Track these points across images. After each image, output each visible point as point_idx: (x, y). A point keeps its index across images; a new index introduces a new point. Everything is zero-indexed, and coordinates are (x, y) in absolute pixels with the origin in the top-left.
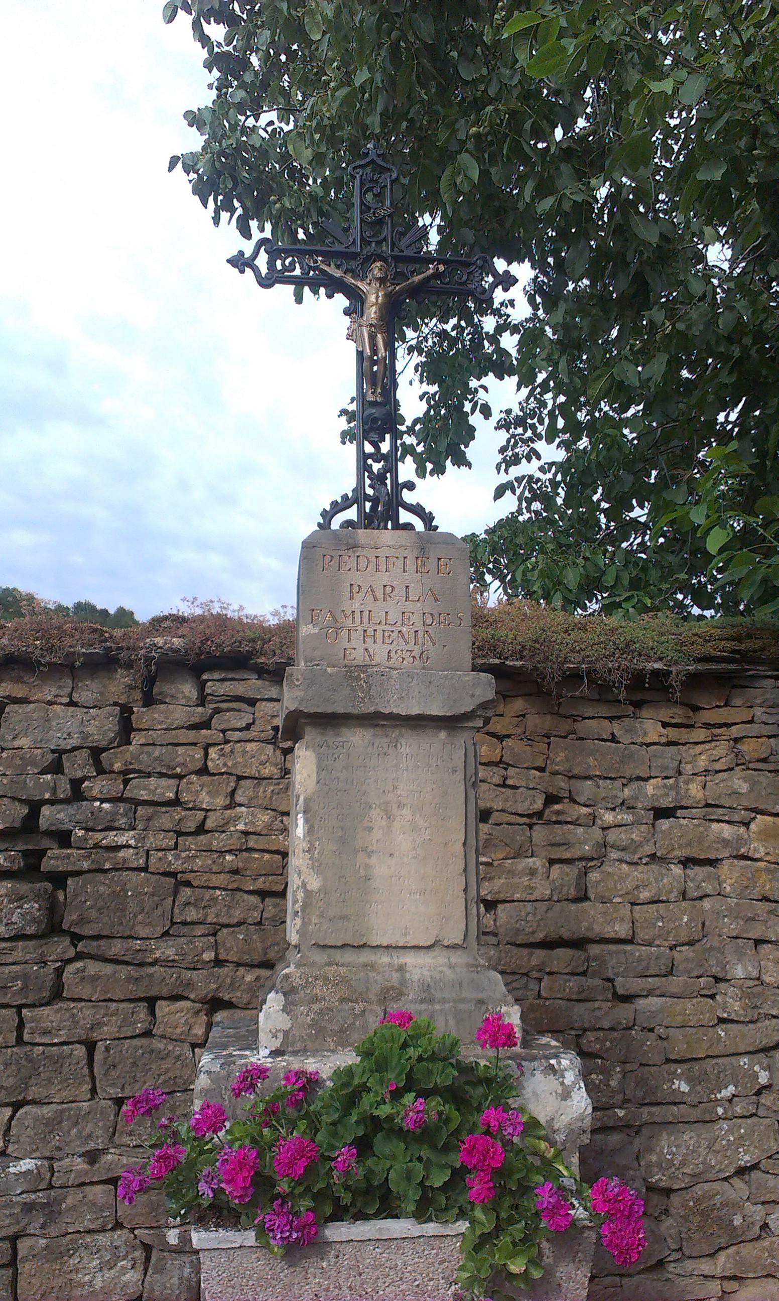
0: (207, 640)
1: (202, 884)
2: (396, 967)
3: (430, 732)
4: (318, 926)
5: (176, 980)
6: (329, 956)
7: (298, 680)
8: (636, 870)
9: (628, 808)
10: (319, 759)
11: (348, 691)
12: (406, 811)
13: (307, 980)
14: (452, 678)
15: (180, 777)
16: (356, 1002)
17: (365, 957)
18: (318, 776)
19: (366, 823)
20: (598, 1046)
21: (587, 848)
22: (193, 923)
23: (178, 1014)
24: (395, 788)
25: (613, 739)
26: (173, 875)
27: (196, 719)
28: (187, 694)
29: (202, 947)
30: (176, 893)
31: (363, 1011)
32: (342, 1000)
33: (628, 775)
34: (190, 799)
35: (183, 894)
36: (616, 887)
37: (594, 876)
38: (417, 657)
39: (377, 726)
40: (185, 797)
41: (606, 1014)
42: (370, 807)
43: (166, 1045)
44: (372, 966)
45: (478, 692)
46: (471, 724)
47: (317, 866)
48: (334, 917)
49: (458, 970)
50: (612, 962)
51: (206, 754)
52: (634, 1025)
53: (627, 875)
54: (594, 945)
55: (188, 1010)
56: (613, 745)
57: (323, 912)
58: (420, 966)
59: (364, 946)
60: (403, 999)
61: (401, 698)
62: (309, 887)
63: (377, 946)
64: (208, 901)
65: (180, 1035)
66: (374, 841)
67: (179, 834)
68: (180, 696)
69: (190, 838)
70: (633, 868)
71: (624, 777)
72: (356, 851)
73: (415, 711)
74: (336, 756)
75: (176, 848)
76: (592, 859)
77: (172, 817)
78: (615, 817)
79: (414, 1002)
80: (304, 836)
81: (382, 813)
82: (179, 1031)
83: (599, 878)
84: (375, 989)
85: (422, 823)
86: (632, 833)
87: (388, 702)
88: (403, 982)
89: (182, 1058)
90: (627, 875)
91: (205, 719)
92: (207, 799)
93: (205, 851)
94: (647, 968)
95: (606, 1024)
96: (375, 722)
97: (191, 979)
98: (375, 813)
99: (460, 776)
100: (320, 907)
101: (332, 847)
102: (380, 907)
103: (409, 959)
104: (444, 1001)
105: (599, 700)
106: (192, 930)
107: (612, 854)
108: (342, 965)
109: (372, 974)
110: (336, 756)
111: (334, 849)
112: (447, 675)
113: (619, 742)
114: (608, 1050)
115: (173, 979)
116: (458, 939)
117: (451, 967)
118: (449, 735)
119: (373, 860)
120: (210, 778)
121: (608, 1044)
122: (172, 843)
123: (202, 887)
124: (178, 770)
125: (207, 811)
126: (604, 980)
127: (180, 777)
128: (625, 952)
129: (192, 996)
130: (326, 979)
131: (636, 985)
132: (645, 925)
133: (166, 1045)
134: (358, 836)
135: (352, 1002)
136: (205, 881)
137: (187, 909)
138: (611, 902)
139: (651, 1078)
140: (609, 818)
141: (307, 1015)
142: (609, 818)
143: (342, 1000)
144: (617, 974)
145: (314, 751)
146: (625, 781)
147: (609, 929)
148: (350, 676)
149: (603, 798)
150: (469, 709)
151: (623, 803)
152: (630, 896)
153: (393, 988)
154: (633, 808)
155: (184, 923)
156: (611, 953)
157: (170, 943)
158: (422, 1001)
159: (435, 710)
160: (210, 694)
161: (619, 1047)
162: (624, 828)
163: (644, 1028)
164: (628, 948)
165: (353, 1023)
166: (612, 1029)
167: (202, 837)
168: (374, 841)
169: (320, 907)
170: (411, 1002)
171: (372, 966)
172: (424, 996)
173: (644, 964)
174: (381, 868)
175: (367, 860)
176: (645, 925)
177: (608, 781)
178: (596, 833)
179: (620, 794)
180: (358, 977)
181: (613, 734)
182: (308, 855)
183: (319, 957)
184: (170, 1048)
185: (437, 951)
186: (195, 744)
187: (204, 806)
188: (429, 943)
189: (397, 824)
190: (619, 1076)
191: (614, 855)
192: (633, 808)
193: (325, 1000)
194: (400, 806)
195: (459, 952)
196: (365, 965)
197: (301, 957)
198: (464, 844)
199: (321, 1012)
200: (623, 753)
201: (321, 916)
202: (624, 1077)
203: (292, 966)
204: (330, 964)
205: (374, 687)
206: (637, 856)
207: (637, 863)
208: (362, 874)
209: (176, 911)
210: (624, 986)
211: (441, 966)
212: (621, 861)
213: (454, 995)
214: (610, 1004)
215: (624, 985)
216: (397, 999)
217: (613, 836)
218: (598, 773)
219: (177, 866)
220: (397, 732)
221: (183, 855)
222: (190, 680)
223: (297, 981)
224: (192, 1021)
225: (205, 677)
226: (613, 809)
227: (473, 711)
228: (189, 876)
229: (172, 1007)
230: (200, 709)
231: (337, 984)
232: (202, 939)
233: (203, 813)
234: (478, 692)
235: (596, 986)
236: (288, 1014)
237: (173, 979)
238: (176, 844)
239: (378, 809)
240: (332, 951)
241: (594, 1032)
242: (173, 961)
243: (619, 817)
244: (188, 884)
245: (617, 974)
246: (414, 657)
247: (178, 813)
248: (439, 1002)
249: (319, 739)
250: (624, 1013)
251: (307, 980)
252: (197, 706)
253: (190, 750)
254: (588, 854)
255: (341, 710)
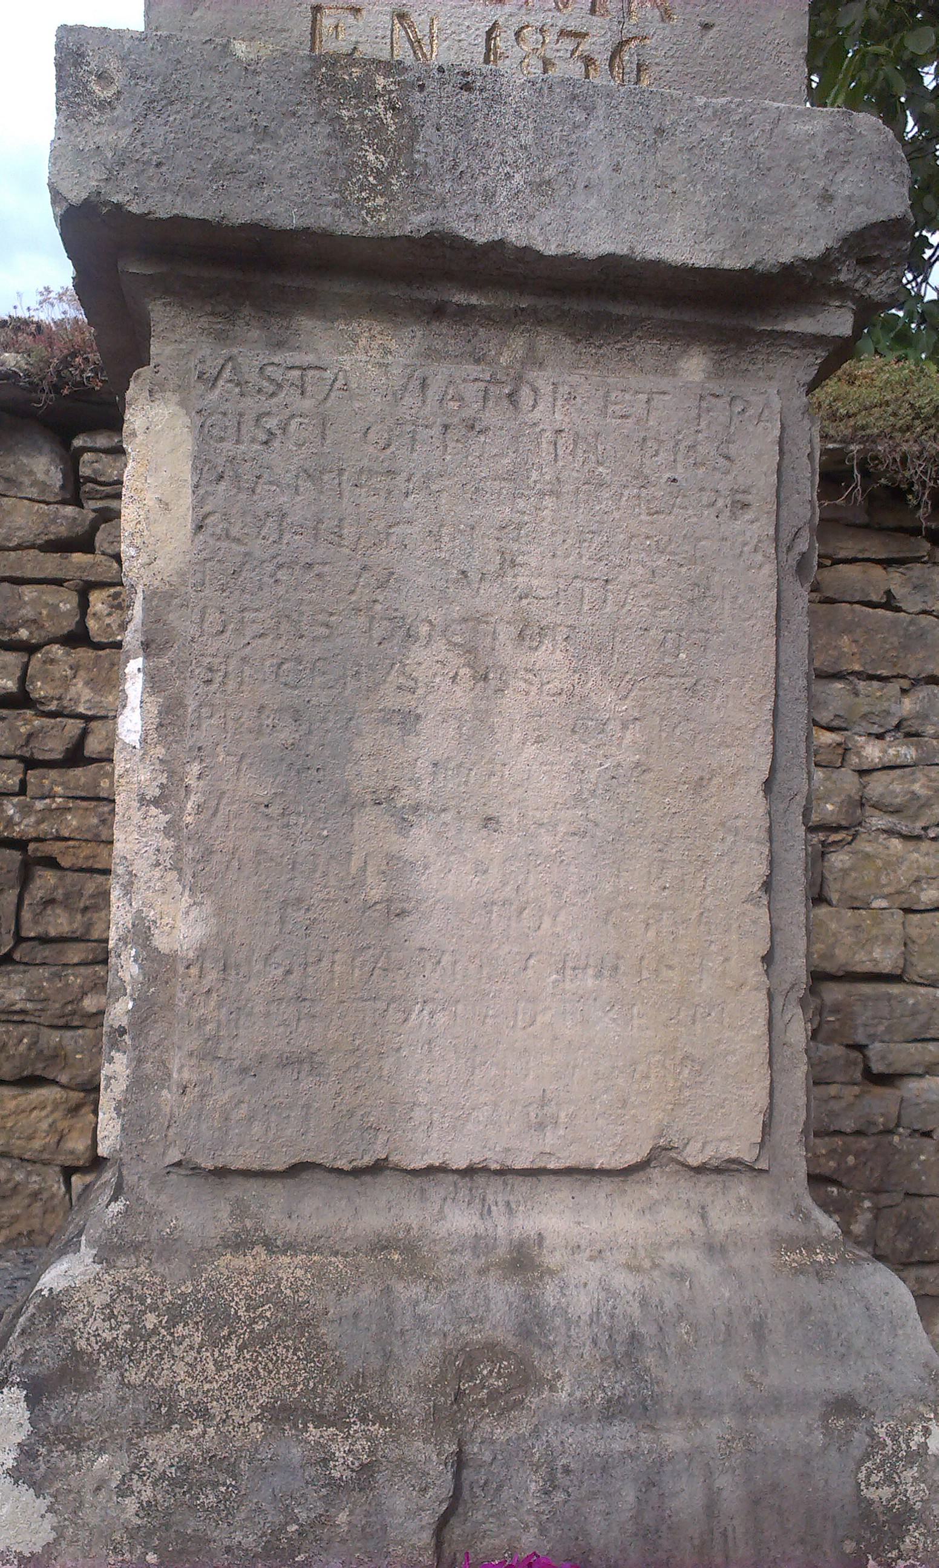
0: (74, 355)
1: (80, 863)
2: (502, 1251)
3: (646, 350)
4: (193, 1093)
5: (29, 1049)
6: (240, 1210)
7: (103, 77)
8: (917, 851)
9: (908, 735)
10: (204, 434)
11: (316, 140)
12: (550, 656)
13: (136, 1321)
14: (745, 123)
15: (29, 649)
16: (337, 1419)
17: (378, 1212)
18: (199, 503)
19: (391, 699)
20: (832, 1164)
21: (829, 807)
22: (62, 940)
23: (35, 1113)
24: (509, 562)
25: (889, 603)
26: (19, 844)
27: (60, 530)
28: (41, 476)
29: (82, 987)
30: (25, 879)
31: (366, 1471)
32: (280, 1415)
33: (912, 672)
34: (51, 693)
35: (38, 882)
36: (878, 880)
37: (839, 859)
38: (602, 59)
39: (438, 312)
40: (39, 689)
41: (851, 1105)
42: (410, 635)
43: (11, 1171)
44: (410, 1249)
45: (849, 183)
46: (806, 325)
47: (195, 861)
48: (262, 1059)
49: (740, 1260)
50: (864, 1016)
51: (84, 605)
52: (898, 1125)
53: (900, 860)
54: (832, 985)
55: (56, 1106)
56: (889, 613)
57: (216, 1039)
58: (599, 1253)
59: (378, 1168)
60: (533, 1401)
61: (542, 187)
62: (161, 942)
63: (430, 1171)
64: (92, 896)
65: (41, 1152)
66: (423, 767)
67: (31, 764)
68: (27, 481)
69: (53, 774)
70: (911, 845)
71: (904, 677)
72: (350, 805)
73: (596, 241)
74: (272, 423)
75: (23, 790)
76: (838, 828)
77: (12, 729)
78: (885, 752)
79: (577, 1414)
80: (144, 741)
81: (455, 660)
82: (37, 1144)
83: (848, 865)
84: (419, 1358)
85: (607, 701)
86: (914, 781)
87: (489, 196)
88: (532, 1325)
89: (45, 1196)
90: (900, 860)
91: (80, 530)
92: (87, 694)
93: (83, 799)
94: (927, 1026)
95: (848, 1125)
96: (430, 295)
97: (61, 1046)
98: (428, 659)
99: (756, 527)
100: (202, 1022)
101: (254, 786)
102: (441, 1019)
103: (553, 1220)
104: (696, 1408)
105: (866, 527)
106: (60, 952)
107: (874, 821)
108: (291, 1248)
109: (407, 1291)
110: (272, 423)
111: (263, 793)
112: (726, 110)
113: (899, 610)
114: (850, 1170)
115: (22, 1048)
116: (738, 1140)
117: (714, 1249)
118: (718, 372)
119: (420, 841)
120: (91, 653)
121: (851, 1160)
122: (13, 782)
123: (81, 870)
124: (24, 634)
125: (88, 719)
126: (848, 1046)
127: (29, 649)
128: (889, 997)
129: (63, 1078)
130: (218, 1321)
131: (905, 1054)
132: (928, 949)
133: (11, 1171)
134: (357, 745)
135: (321, 1420)
136: (87, 858)
137: (49, 912)
138: (868, 907)
139: (924, 1219)
140: (873, 752)
141: (124, 1490)
142: (873, 752)
143: (280, 1415)
144: (873, 1037)
145: (182, 404)
146: (905, 683)
147: (861, 956)
148: (331, 80)
149: (864, 716)
150: (812, 249)
151: (898, 727)
152: (903, 897)
153: (492, 1350)
154: (917, 735)
155: (44, 940)
156: (864, 999)
157: (16, 978)
158: (613, 1410)
159: (681, 242)
160: (89, 480)
161: (869, 1164)
162: (898, 772)
163: (915, 1131)
164: (895, 989)
165: (324, 1521)
166: (859, 1133)
167: (78, 771)
168: (423, 767)
169: (202, 1022)
170: (567, 1416)
171: (403, 1254)
172: (618, 1384)
173: (922, 1018)
174: (447, 872)
175: (394, 842)
176: (928, 949)
177: (875, 684)
178: (848, 781)
179: (894, 708)
180: (349, 1303)
181: (888, 593)
182: (159, 818)
183: (197, 1216)
184: (19, 1176)
185: (658, 1185)
186: (59, 582)
187: (81, 709)
188: (631, 1158)
189: (513, 703)
190: (869, 1216)
191: (878, 821)
192: (917, 735)
193: (205, 1414)
194: (528, 633)
195: (741, 1188)
196: (381, 1245)
197: (127, 1213)
198: (768, 786)
199: (185, 1478)
200: (906, 630)
201: (206, 1054)
202: (876, 1218)
203: (87, 1253)
204: (239, 1244)
205: (428, 132)
206: (919, 824)
207: (918, 838)
208: (375, 894)
209: (26, 915)
210: (883, 1058)
211: (675, 1244)
212: (890, 832)
213: (736, 1377)
214: (856, 1090)
215: (883, 1055)
216: (503, 1402)
217: (878, 786)
218: (857, 667)
219: (25, 827)
220: (518, 344)
221: (39, 805)
222: (47, 447)
223: (92, 1330)
224: (63, 1125)
225: (78, 442)
226: (880, 737)
227: (825, 263)
228: (53, 849)
229: (22, 1099)
230: (69, 510)
231: (263, 1340)
232: (82, 970)
233: (80, 724)
234: (849, 183)
235: (836, 1058)
236: (38, 1487)
237: (22, 1048)
238: (23, 784)
239: (440, 644)
240: (254, 1187)
241: (827, 1139)
242: (22, 1012)
243: (892, 751)
244: (51, 863)
245: (873, 1037)
246: (588, 61)
247: (26, 722)
248: (679, 1412)
249: (207, 353)
250: (881, 1104)
251: (136, 1321)
252: (64, 502)
253: (49, 595)
254: (832, 820)
255: (284, 211)
